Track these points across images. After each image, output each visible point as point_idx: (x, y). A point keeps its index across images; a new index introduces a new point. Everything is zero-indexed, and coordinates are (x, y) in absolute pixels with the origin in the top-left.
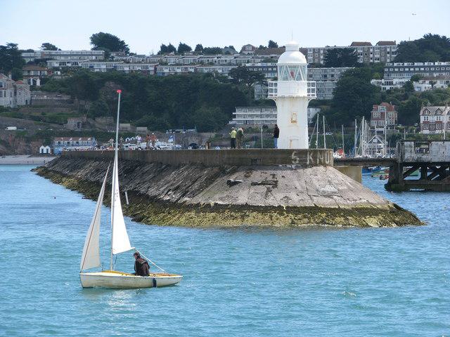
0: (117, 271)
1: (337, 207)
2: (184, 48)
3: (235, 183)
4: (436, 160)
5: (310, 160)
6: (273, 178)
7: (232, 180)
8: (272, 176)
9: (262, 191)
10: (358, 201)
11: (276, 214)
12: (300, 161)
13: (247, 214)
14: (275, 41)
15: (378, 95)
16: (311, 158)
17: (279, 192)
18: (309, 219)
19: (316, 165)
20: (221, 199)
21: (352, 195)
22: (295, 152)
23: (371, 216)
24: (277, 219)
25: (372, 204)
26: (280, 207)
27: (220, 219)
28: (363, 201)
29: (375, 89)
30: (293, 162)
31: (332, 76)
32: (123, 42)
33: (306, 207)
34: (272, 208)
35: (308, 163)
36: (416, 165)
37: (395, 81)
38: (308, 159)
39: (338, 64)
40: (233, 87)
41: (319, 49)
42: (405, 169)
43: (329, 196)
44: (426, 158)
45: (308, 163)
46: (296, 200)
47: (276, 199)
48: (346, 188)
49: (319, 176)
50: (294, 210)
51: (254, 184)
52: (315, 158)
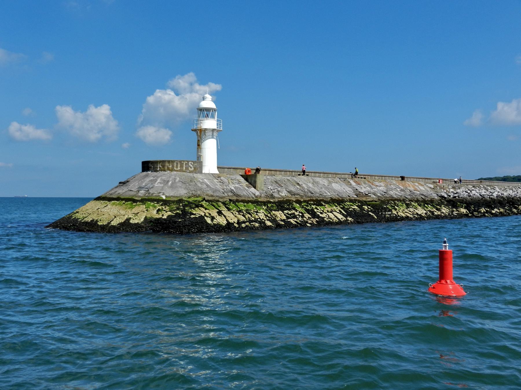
5: (160, 167)
16: (161, 166)
19: (165, 171)
45: (158, 169)
52: (163, 166)
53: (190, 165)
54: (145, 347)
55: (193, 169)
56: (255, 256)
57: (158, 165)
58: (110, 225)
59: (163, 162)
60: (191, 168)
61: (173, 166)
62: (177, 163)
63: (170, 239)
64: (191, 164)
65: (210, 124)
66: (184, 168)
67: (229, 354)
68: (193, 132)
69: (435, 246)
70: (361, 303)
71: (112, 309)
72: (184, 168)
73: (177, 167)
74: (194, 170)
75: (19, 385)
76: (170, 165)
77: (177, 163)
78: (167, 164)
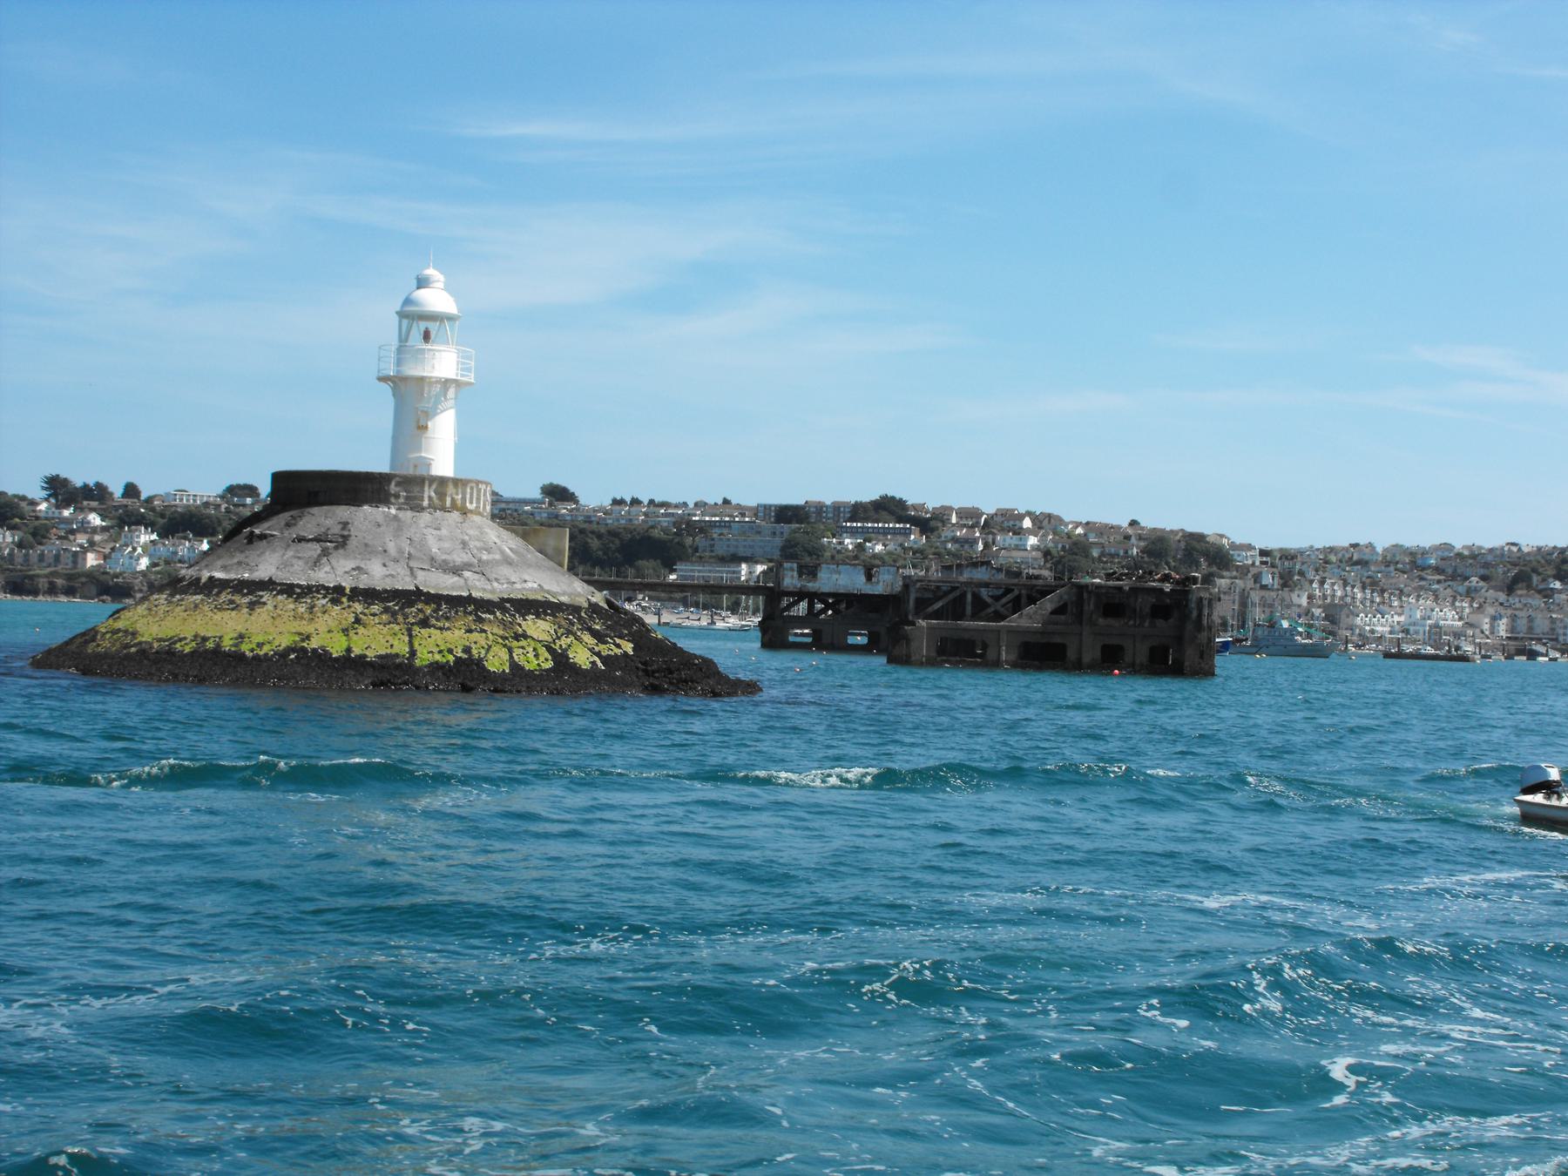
0: (362, 756)
1: (465, 594)
2: (636, 502)
3: (263, 537)
4: (826, 589)
5: (430, 498)
6: (343, 529)
7: (257, 531)
8: (340, 526)
9: (310, 553)
10: (518, 586)
11: (324, 602)
12: (407, 498)
13: (264, 600)
14: (729, 498)
15: (828, 554)
16: (433, 494)
17: (346, 557)
18: (394, 614)
19: (443, 509)
20: (224, 568)
21: (505, 571)
22: (397, 479)
23: (538, 616)
24: (324, 612)
25: (548, 592)
26: (339, 590)
27: (206, 608)
28: (530, 585)
29: (823, 548)
30: (393, 500)
31: (782, 533)
32: (573, 494)
33: (397, 591)
34: (320, 588)
35: (426, 503)
36: (801, 595)
37: (847, 541)
38: (426, 495)
39: (789, 521)
40: (676, 540)
41: (770, 506)
42: (785, 603)
43: (456, 571)
44: (812, 586)
45: (426, 503)
46: (378, 575)
47: (337, 571)
48: (498, 557)
49: (444, 532)
50: (369, 595)
51: (301, 540)
52: (441, 495)
56: (1120, 849)
57: (426, 488)
58: (90, 649)
59: (478, 482)
63: (161, 695)
65: (443, 362)
68: (382, 383)
71: (28, 926)
76: (457, 494)
78: (451, 489)
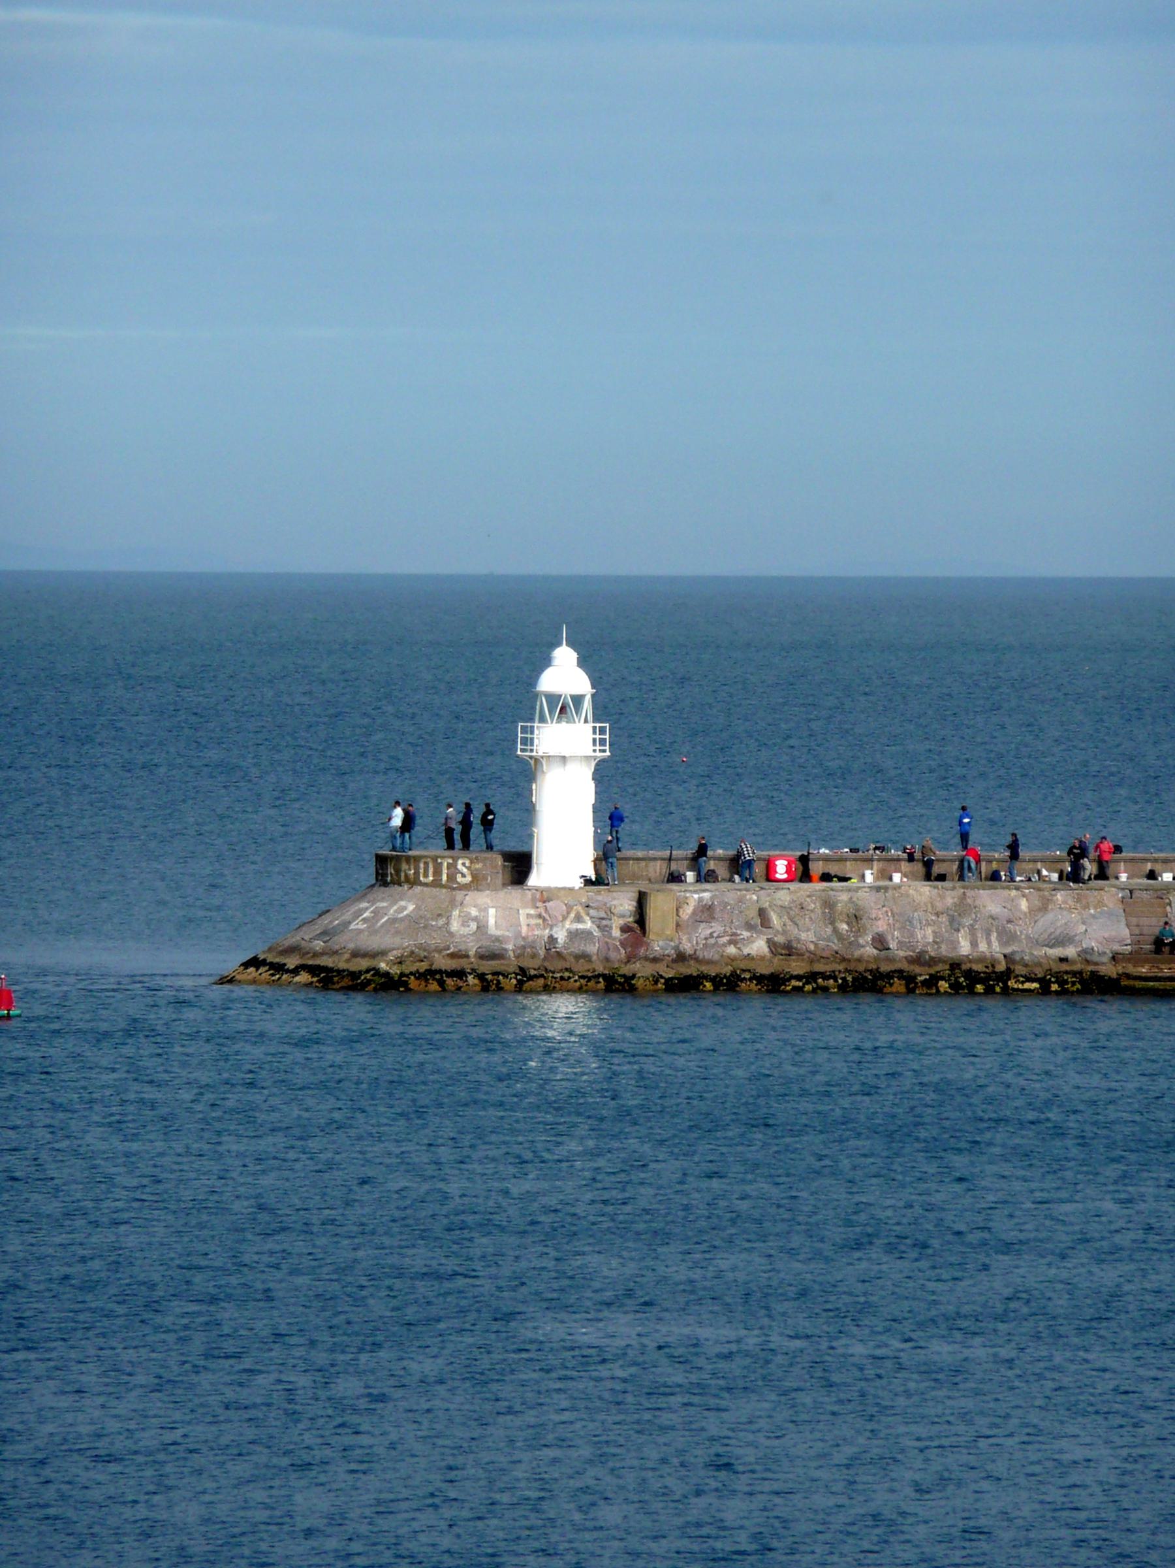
19: (400, 884)
53: (460, 867)
54: (469, 1019)
55: (469, 879)
60: (464, 876)
61: (417, 873)
62: (426, 864)
64: (464, 864)
66: (444, 877)
67: (822, 851)
69: (1045, 1195)
70: (689, 978)
72: (444, 877)
73: (426, 876)
74: (472, 882)
75: (310, 1566)
77: (426, 864)
